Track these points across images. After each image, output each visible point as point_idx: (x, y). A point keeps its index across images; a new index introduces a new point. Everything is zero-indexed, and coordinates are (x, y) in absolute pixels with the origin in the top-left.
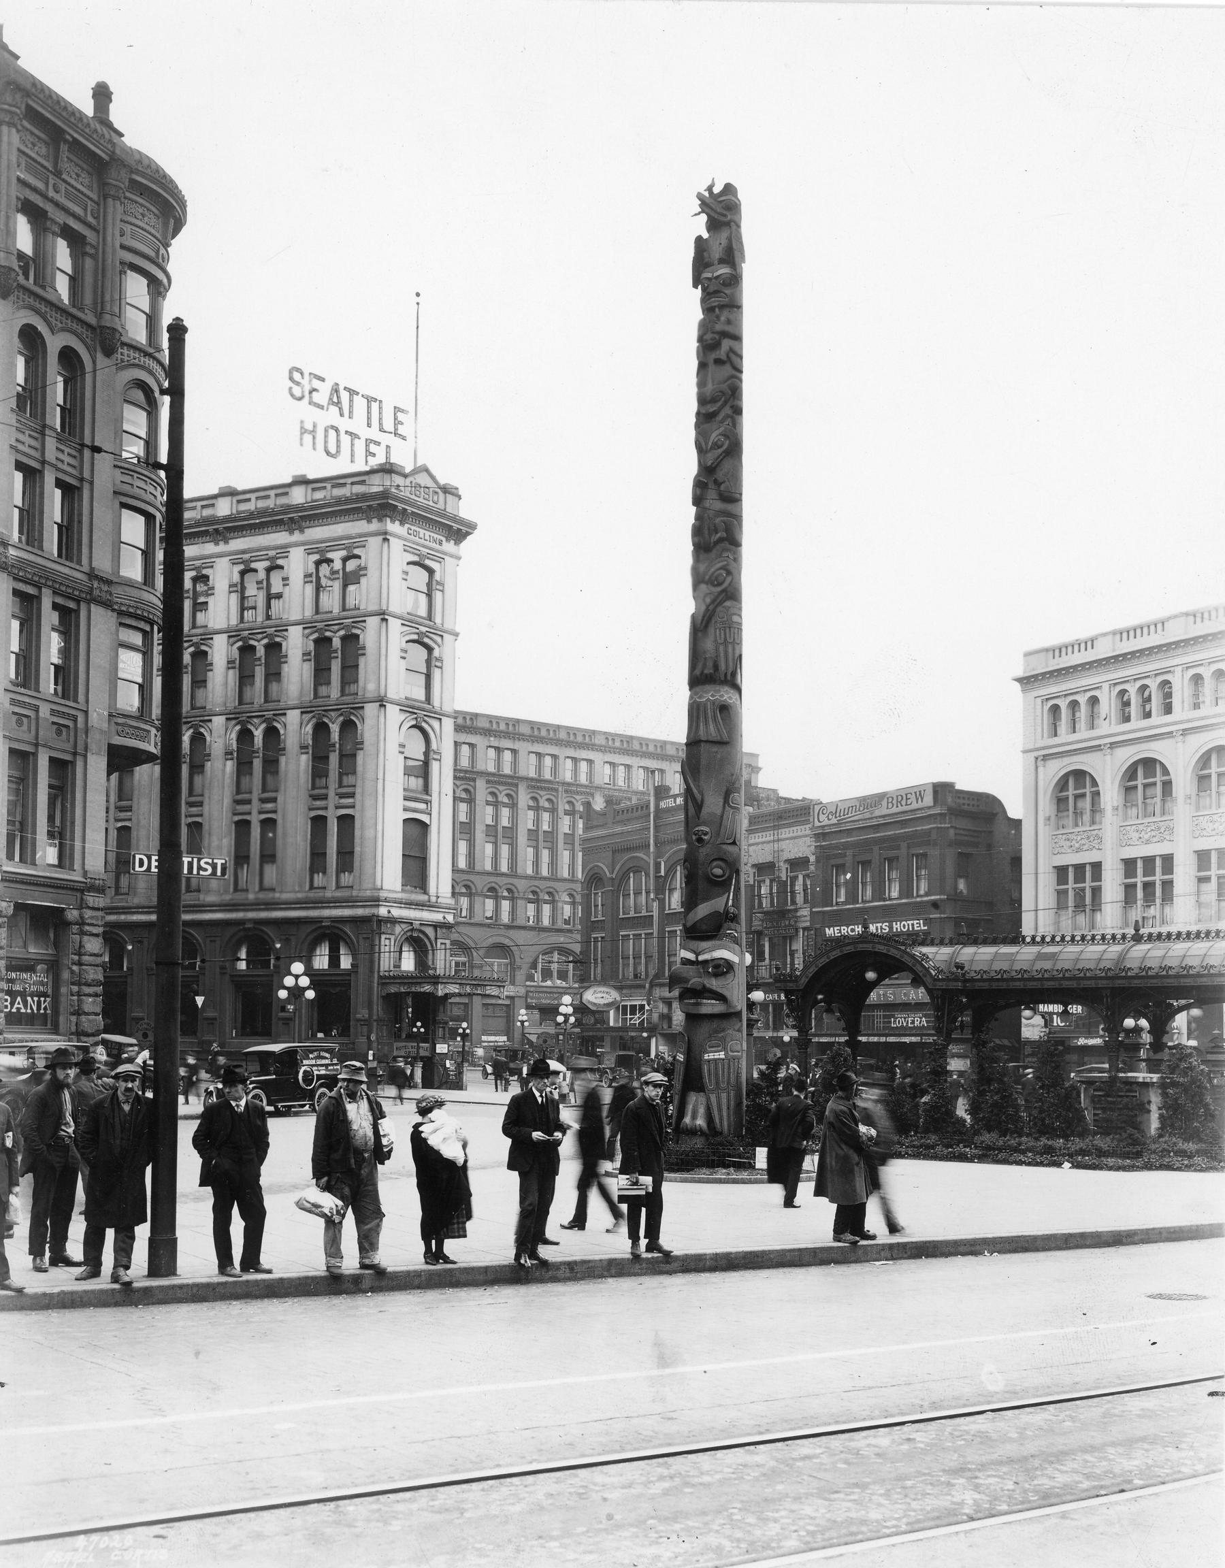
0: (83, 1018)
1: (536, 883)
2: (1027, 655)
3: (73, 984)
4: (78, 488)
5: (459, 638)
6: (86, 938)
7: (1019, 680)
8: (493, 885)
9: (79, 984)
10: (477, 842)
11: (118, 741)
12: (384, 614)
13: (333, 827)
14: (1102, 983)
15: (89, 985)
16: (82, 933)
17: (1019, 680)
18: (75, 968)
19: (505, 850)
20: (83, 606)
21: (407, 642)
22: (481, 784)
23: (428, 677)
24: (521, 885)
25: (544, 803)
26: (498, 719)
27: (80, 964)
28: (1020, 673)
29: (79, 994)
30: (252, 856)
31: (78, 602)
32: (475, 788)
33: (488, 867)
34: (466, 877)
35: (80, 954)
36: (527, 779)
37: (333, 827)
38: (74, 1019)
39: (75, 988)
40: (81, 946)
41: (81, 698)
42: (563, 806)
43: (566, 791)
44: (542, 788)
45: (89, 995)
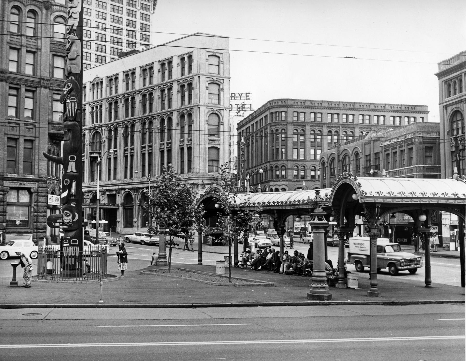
0: (38, 224)
1: (314, 163)
2: (439, 64)
3: (35, 212)
4: (37, 52)
5: (230, 79)
6: (39, 197)
7: (436, 75)
8: (276, 165)
9: (37, 212)
10: (307, 149)
11: (52, 131)
12: (198, 75)
13: (186, 150)
14: (378, 201)
15: (41, 213)
16: (38, 196)
17: (436, 75)
18: (35, 207)
19: (302, 151)
20: (38, 89)
21: (209, 84)
22: (308, 128)
23: (219, 95)
24: (308, 164)
25: (317, 132)
26: (315, 102)
27: (37, 206)
28: (437, 71)
29: (37, 216)
30: (185, 160)
31: (36, 88)
32: (306, 129)
33: (312, 158)
34: (303, 163)
35: (37, 203)
36: (327, 124)
37: (186, 150)
38: (35, 224)
39: (36, 214)
40: (37, 200)
41: (37, 119)
42: (342, 133)
43: (343, 127)
44: (333, 127)
45: (41, 216)
